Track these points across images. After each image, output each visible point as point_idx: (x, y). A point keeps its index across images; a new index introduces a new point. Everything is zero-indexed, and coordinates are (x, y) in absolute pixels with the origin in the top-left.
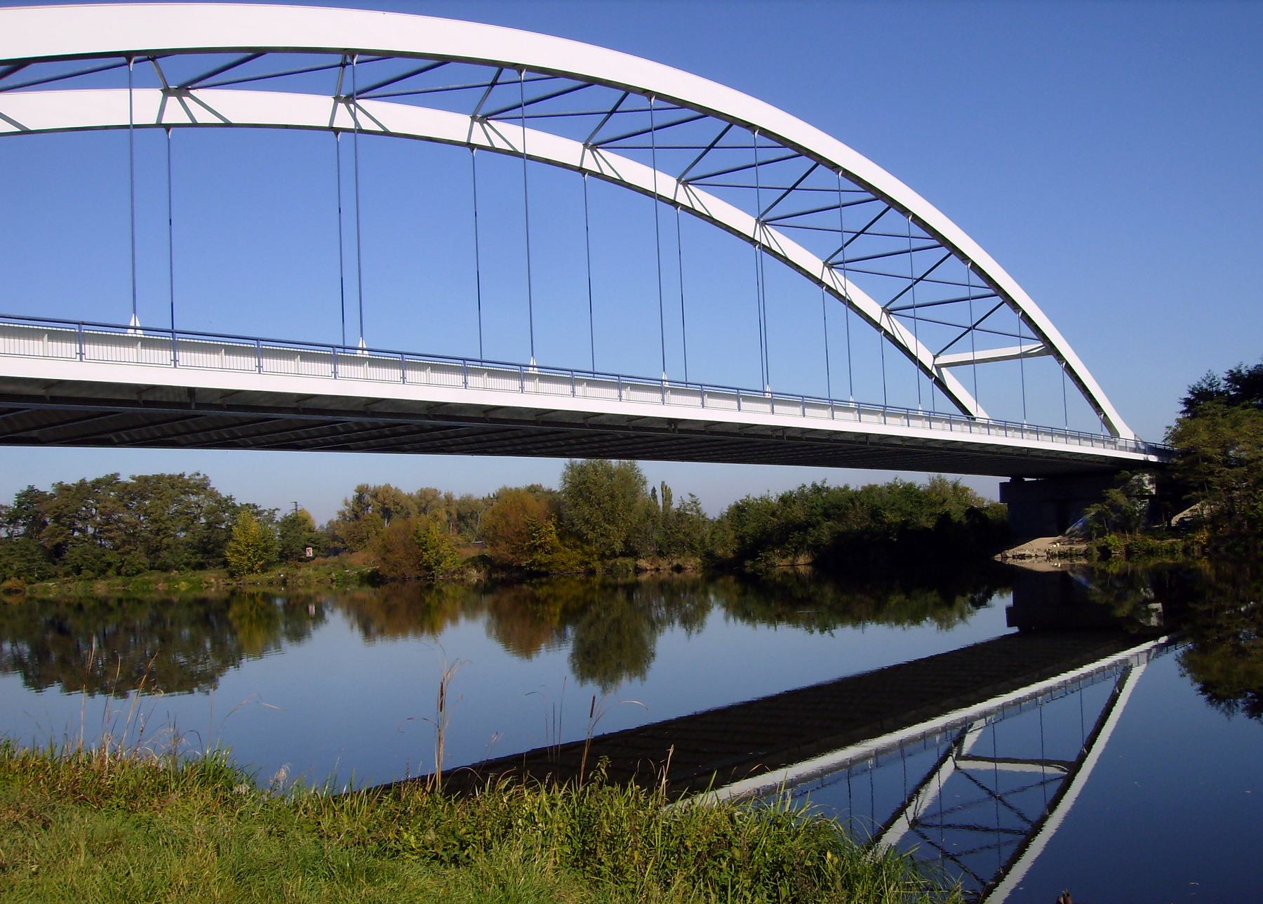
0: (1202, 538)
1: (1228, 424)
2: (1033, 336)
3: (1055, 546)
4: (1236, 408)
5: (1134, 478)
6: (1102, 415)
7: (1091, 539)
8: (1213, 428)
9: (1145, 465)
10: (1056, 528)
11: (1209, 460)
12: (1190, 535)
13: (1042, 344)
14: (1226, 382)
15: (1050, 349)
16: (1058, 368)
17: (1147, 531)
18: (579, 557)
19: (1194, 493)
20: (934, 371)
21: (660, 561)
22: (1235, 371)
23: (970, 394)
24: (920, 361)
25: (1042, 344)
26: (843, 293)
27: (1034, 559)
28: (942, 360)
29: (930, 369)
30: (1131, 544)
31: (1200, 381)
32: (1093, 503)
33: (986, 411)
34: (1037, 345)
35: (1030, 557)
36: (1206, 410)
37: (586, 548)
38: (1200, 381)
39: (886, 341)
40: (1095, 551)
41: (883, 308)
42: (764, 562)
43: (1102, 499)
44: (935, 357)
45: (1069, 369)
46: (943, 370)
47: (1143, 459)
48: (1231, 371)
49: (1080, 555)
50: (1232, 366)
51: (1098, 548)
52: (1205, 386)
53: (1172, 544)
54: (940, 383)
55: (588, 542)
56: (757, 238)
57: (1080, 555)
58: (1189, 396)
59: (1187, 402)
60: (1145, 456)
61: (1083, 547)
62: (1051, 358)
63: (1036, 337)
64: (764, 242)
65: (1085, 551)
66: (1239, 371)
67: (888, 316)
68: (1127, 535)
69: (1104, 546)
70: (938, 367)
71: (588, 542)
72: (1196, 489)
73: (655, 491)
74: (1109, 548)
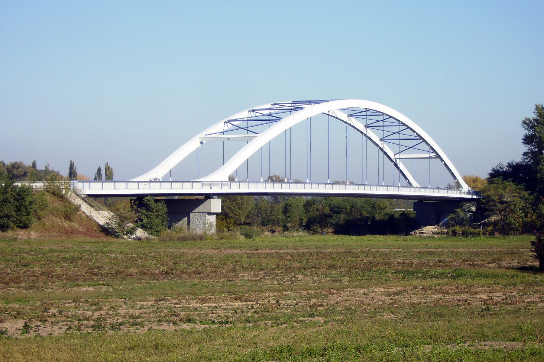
0: (490, 229)
1: (502, 188)
2: (432, 151)
3: (435, 229)
4: (506, 182)
5: (467, 205)
6: (456, 180)
7: (449, 228)
8: (496, 189)
9: (472, 200)
10: (436, 222)
11: (494, 201)
12: (486, 228)
13: (435, 155)
14: (507, 167)
15: (438, 156)
16: (442, 164)
17: (470, 225)
18: (225, 224)
19: (488, 213)
20: (394, 160)
21: (263, 228)
22: (511, 163)
23: (413, 177)
24: (384, 151)
25: (435, 155)
26: (369, 136)
27: (427, 234)
28: (397, 156)
29: (393, 159)
30: (464, 230)
31: (497, 166)
32: (451, 214)
33: (418, 183)
34: (433, 155)
35: (426, 233)
36: (495, 181)
37: (229, 221)
38: (497, 166)
39: (380, 151)
40: (451, 232)
41: (380, 139)
42: (44, 235)
43: (454, 212)
44: (395, 155)
45: (445, 165)
46: (398, 160)
47: (471, 197)
48: (509, 163)
49: (445, 233)
50: (510, 161)
51: (452, 231)
52: (498, 168)
53: (479, 231)
54: (396, 165)
55: (230, 218)
56: (347, 122)
57: (445, 233)
58: (492, 172)
59: (491, 174)
60: (472, 196)
61: (446, 230)
62: (438, 160)
63: (433, 152)
64: (349, 123)
65: (447, 232)
66: (512, 163)
67: (381, 141)
68: (463, 227)
69: (454, 231)
70: (396, 159)
71: (230, 218)
72: (489, 211)
73: (101, 170)
74: (456, 231)
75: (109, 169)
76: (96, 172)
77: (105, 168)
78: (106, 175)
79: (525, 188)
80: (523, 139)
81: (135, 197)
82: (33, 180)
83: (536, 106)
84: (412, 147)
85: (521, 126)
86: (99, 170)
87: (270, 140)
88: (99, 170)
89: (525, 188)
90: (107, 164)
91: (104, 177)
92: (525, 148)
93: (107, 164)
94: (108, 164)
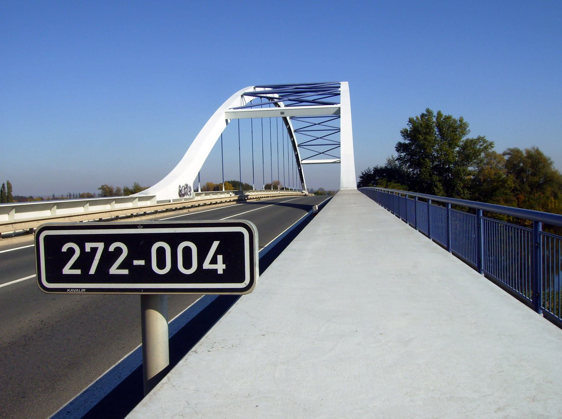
75: (9, 184)
76: (2, 186)
77: (7, 184)
78: (8, 188)
79: (409, 188)
80: (396, 147)
81: (34, 275)
82: (456, 187)
83: (409, 119)
84: (322, 153)
85: (401, 136)
86: (4, 185)
87: (222, 132)
88: (4, 185)
89: (409, 188)
90: (8, 181)
91: (72, 197)
92: (396, 155)
93: (8, 181)
94: (9, 181)
